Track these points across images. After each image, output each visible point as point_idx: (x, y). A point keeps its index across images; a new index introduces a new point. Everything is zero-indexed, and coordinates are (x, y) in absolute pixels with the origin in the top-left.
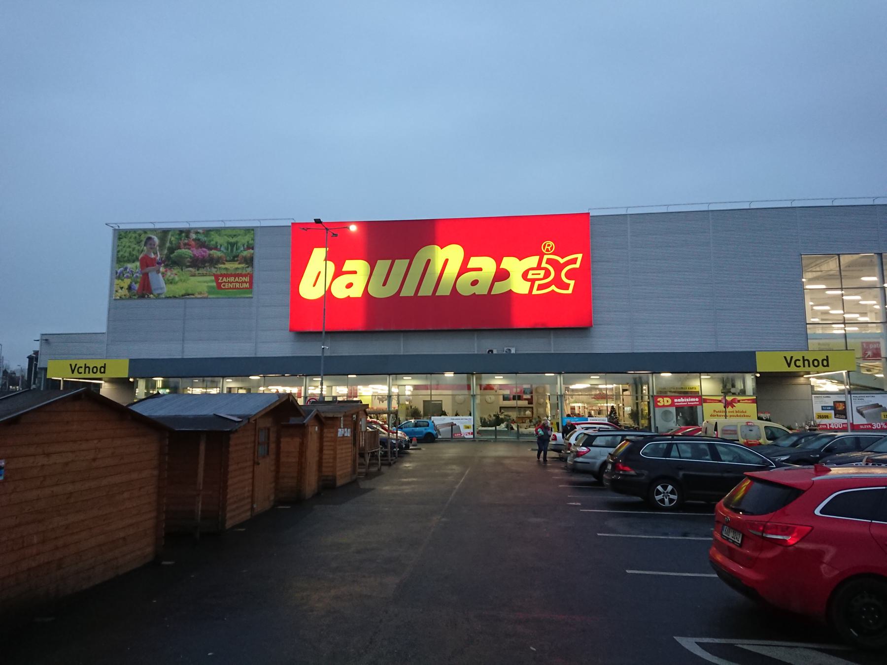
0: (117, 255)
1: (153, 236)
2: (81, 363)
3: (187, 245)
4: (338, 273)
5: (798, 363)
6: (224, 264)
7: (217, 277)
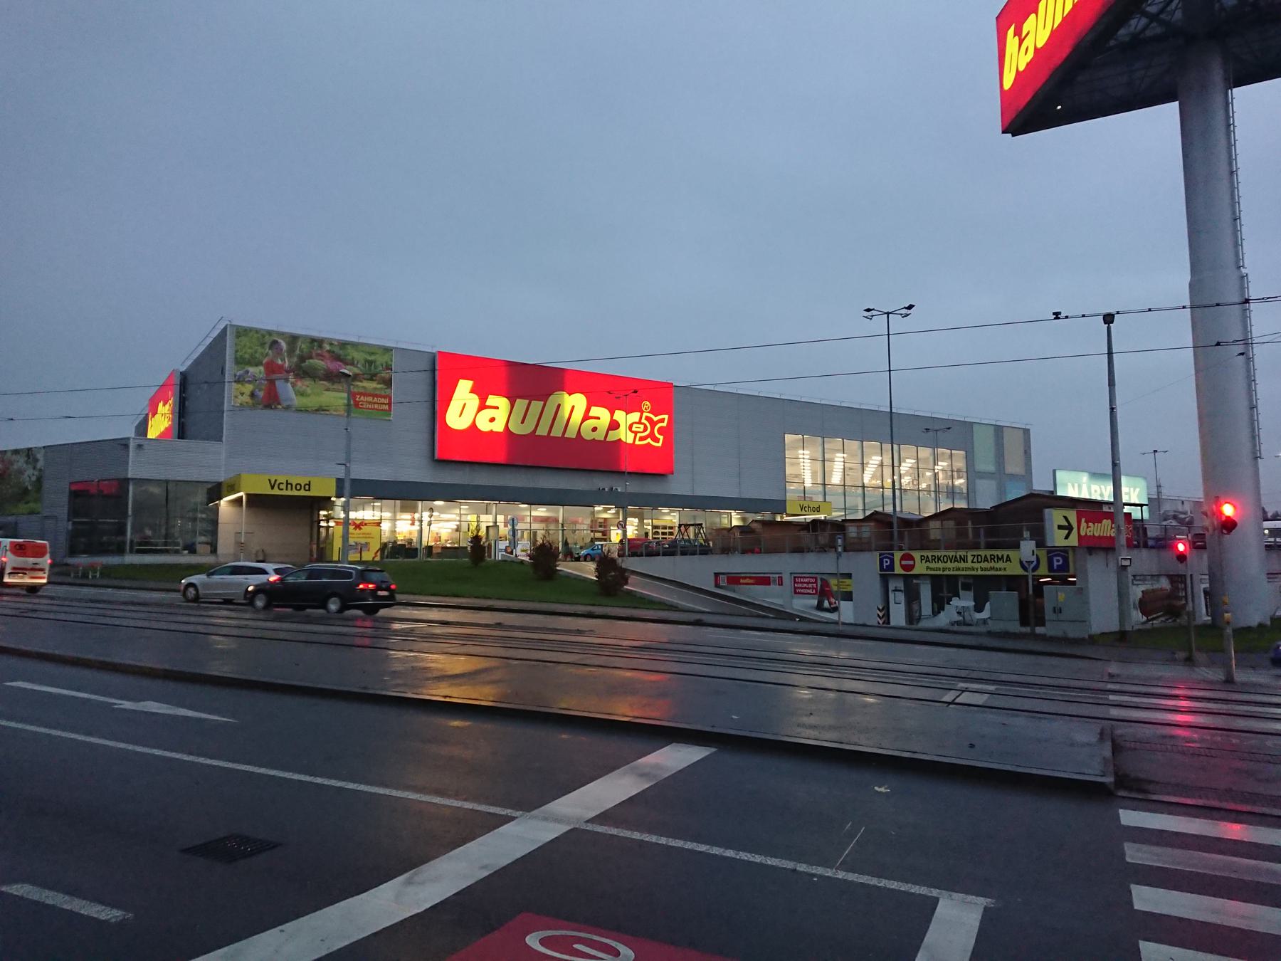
0: (236, 355)
1: (280, 341)
2: (282, 479)
3: (320, 356)
4: (483, 406)
5: (281, 486)
6: (361, 381)
7: (352, 395)
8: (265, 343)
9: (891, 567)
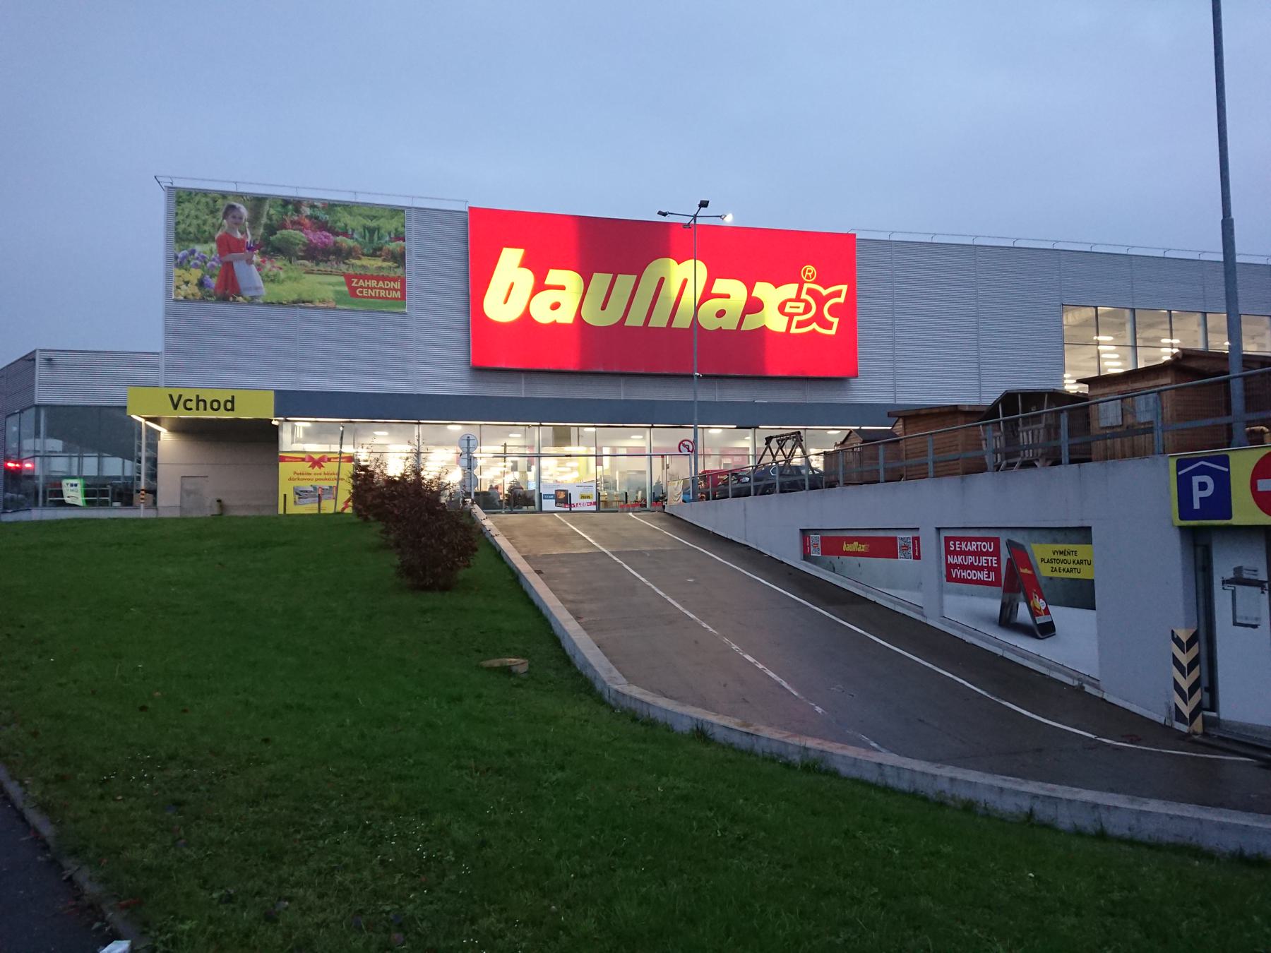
0: (176, 229)
1: (238, 205)
2: (189, 394)
3: (297, 225)
4: (540, 286)
5: (189, 405)
6: (360, 259)
7: (349, 279)
8: (218, 210)
9: (1220, 503)
